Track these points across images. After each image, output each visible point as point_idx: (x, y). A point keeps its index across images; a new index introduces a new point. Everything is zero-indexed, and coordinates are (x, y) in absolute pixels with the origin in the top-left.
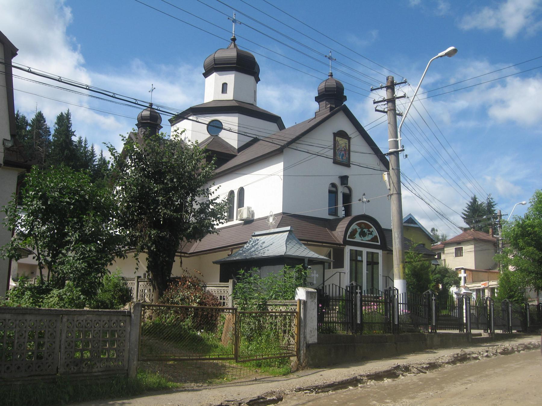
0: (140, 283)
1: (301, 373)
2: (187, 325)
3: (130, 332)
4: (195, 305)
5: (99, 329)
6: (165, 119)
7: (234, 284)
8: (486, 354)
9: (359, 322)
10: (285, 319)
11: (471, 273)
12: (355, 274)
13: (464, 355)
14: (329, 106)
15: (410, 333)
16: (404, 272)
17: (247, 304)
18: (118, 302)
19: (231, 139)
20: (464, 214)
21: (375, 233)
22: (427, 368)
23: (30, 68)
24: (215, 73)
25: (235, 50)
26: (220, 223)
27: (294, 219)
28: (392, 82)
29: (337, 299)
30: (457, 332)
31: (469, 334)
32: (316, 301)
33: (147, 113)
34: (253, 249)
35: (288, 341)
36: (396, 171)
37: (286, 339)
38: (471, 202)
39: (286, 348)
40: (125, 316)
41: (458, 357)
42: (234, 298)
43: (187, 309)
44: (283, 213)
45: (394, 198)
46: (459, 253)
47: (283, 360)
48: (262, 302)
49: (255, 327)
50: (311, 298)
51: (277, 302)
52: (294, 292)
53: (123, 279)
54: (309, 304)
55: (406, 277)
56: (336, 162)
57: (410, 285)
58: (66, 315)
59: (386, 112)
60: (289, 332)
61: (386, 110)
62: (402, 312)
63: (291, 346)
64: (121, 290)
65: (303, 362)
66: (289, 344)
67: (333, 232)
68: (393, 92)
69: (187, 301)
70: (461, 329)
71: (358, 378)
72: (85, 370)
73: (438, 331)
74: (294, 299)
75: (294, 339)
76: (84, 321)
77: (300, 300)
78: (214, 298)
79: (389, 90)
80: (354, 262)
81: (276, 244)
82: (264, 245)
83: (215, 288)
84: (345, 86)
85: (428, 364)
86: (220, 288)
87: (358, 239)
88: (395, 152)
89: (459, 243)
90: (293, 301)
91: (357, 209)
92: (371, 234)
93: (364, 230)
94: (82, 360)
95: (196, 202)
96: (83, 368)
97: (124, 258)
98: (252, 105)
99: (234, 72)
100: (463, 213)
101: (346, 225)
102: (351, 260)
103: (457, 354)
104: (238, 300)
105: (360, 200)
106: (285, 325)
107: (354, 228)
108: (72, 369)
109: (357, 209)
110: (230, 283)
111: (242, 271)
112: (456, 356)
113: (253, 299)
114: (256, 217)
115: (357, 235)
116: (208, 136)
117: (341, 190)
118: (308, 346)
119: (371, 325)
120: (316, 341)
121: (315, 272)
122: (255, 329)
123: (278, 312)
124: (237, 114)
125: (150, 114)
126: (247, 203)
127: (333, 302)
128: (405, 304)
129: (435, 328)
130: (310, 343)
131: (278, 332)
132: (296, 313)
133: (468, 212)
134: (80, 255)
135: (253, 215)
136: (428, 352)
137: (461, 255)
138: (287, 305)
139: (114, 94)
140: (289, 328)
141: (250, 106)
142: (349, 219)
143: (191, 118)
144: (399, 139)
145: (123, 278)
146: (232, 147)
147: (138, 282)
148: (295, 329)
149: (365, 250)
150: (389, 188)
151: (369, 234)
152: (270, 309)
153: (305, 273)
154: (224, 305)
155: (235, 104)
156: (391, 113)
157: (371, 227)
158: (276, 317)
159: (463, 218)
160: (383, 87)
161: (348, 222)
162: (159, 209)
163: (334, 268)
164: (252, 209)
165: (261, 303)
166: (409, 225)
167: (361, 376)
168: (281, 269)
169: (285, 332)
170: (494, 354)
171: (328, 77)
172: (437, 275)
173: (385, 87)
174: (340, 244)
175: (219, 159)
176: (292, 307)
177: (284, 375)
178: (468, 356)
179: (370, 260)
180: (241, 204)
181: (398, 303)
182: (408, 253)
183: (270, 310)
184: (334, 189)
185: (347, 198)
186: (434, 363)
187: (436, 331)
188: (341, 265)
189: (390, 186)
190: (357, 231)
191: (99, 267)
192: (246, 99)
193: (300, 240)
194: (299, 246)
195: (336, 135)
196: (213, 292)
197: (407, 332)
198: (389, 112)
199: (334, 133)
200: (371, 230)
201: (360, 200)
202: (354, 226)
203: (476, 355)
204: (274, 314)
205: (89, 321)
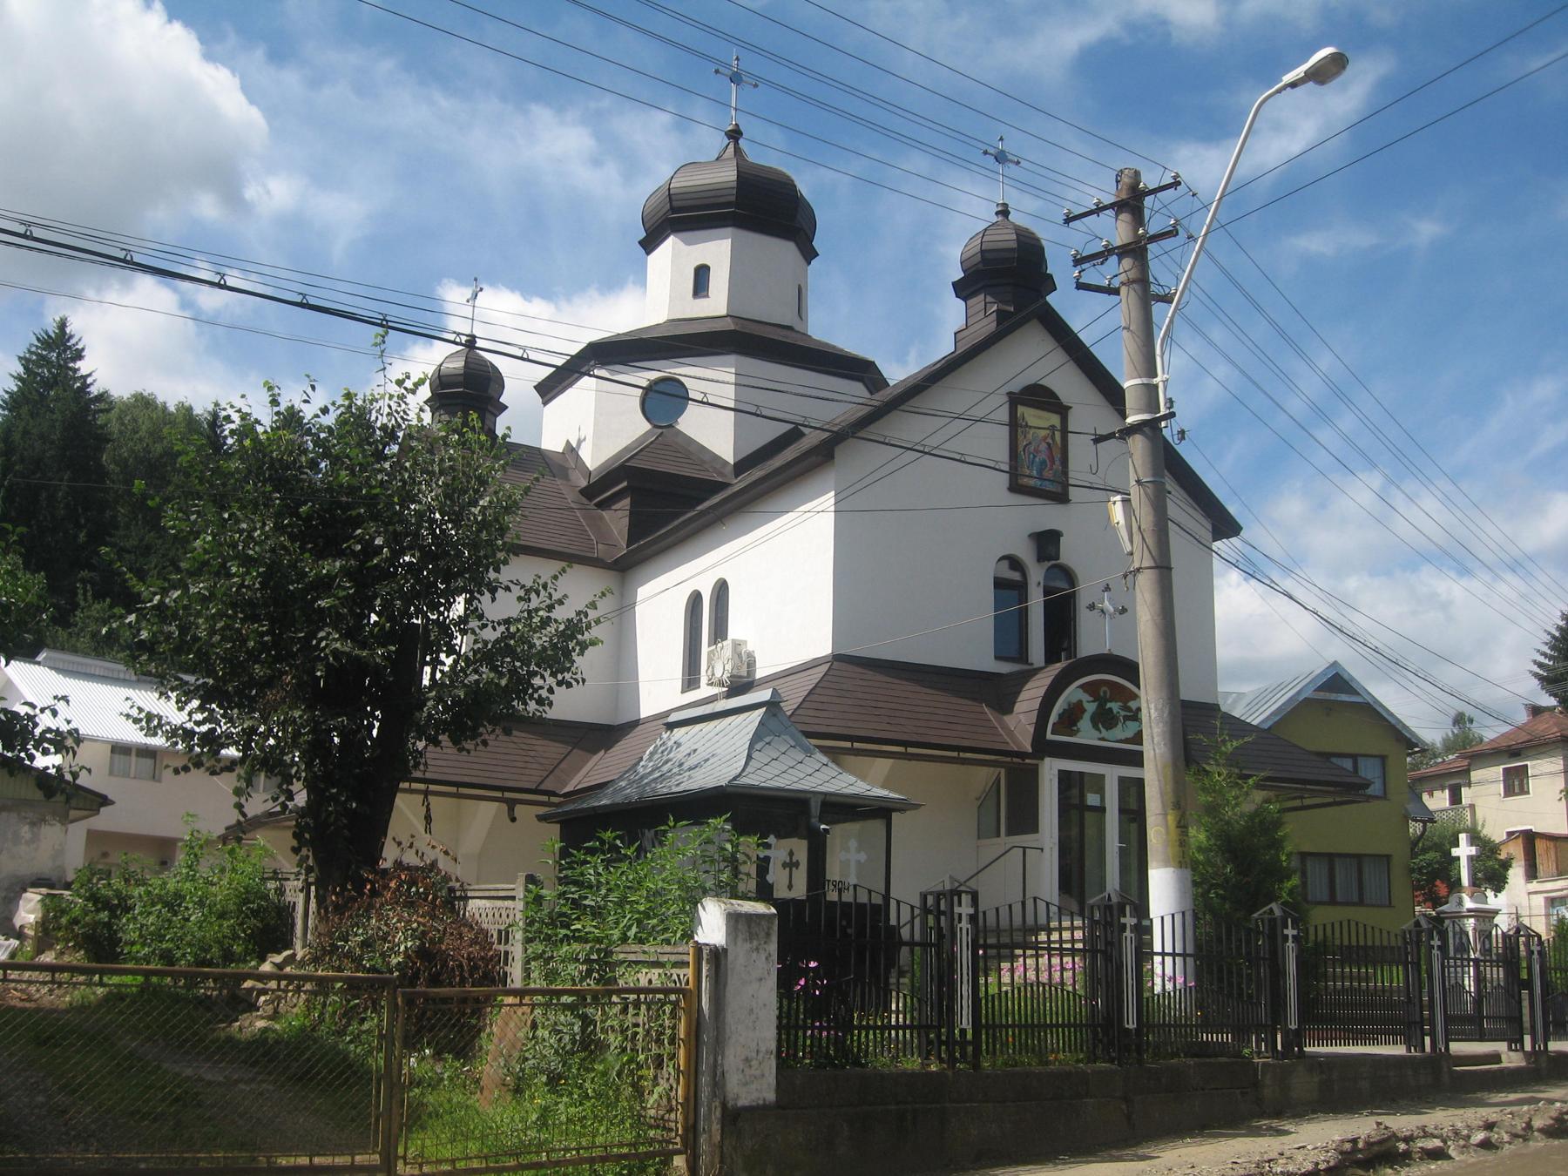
6: (518, 382)
8: (1479, 1136)
11: (1551, 844)
13: (1380, 1142)
15: (1191, 1061)
16: (1183, 843)
18: (246, 952)
19: (713, 431)
20: (1540, 665)
23: (304, 296)
26: (559, 684)
27: (869, 674)
30: (1399, 1050)
31: (1441, 1060)
32: (773, 947)
36: (1150, 489)
38: (1559, 628)
39: (660, 1123)
41: (1355, 1150)
44: (837, 658)
45: (1145, 585)
46: (1516, 783)
49: (573, 1042)
50: (752, 937)
54: (739, 959)
55: (1183, 859)
59: (1116, 292)
61: (1116, 283)
67: (1006, 718)
68: (1138, 218)
77: (699, 948)
79: (1125, 217)
81: (719, 755)
86: (499, 903)
87: (1086, 735)
88: (1144, 423)
89: (1514, 753)
93: (1109, 705)
98: (790, 328)
99: (729, 230)
100: (1535, 662)
101: (1042, 692)
103: (1354, 1141)
105: (1092, 607)
106: (659, 1042)
112: (1348, 1146)
115: (1085, 724)
116: (647, 426)
117: (1036, 574)
118: (733, 1117)
120: (771, 1096)
121: (853, 844)
124: (732, 358)
125: (466, 366)
126: (734, 631)
127: (1073, 941)
128: (1184, 955)
130: (743, 1102)
133: (1551, 658)
135: (751, 664)
136: (1256, 1132)
137: (1524, 791)
139: (29, 224)
141: (785, 332)
142: (1057, 668)
143: (596, 372)
146: (716, 458)
150: (1129, 548)
151: (1126, 718)
152: (626, 978)
155: (729, 325)
156: (1132, 293)
159: (1536, 675)
160: (1105, 208)
162: (322, 639)
163: (1010, 833)
164: (750, 648)
166: (1333, 696)
170: (1516, 1136)
171: (995, 219)
172: (1430, 855)
173: (1111, 206)
174: (1022, 755)
175: (664, 502)
178: (1402, 1146)
180: (720, 632)
184: (1016, 576)
187: (1301, 1049)
189: (1131, 541)
190: (1083, 711)
192: (771, 310)
193: (809, 735)
194: (800, 756)
195: (1015, 400)
198: (1124, 290)
202: (1072, 693)
203: (1437, 1143)
204: (632, 997)
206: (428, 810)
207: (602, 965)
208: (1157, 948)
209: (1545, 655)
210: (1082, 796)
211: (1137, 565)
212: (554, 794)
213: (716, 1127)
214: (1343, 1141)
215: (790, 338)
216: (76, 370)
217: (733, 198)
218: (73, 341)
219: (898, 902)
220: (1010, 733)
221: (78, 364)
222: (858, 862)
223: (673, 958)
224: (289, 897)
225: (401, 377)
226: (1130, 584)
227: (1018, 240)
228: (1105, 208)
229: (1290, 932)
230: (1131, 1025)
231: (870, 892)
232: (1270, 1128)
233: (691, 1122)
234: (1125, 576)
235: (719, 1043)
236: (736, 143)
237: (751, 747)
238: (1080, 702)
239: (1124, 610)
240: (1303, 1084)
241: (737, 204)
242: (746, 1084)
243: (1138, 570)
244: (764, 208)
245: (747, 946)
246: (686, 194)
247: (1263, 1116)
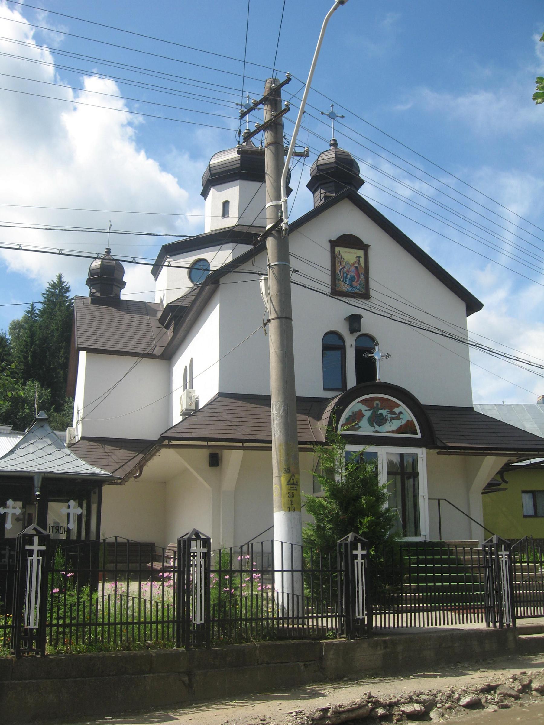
21: (408, 415)
24: (212, 189)
27: (239, 403)
87: (365, 429)
92: (398, 417)
107: (356, 409)
117: (350, 341)
128: (292, 571)
151: (392, 419)
157: (398, 406)
184: (335, 341)
190: (363, 416)
195: (334, 244)
199: (331, 241)
200: (397, 410)
216: (67, 297)
218: (65, 284)
221: (68, 294)
222: (14, 514)
227: (336, 157)
238: (360, 411)
239: (388, 356)
241: (241, 167)
246: (217, 166)
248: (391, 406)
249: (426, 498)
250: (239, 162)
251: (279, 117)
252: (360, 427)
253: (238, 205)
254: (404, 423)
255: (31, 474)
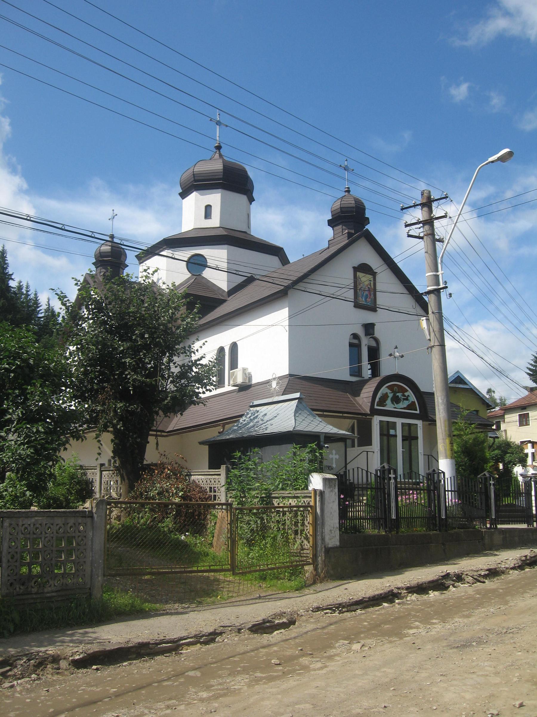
0: (104, 473)
1: (319, 586)
2: (167, 526)
3: (92, 539)
4: (177, 500)
5: (52, 535)
7: (228, 471)
9: (394, 517)
10: (296, 515)
12: (387, 453)
14: (347, 231)
15: (462, 530)
16: (452, 450)
17: (245, 497)
18: (76, 499)
19: (220, 280)
20: (530, 369)
21: (413, 398)
22: (485, 576)
25: (221, 161)
26: (207, 390)
27: (304, 382)
28: (429, 197)
29: (364, 488)
30: (524, 526)
33: (106, 248)
34: (252, 424)
35: (301, 545)
36: (437, 315)
37: (299, 541)
39: (299, 554)
40: (85, 517)
41: (526, 560)
42: (228, 489)
43: (166, 505)
44: (290, 375)
45: (436, 351)
46: (524, 421)
47: (295, 570)
48: (265, 494)
49: (257, 527)
50: (330, 487)
51: (286, 493)
52: (307, 479)
53: (81, 467)
54: (327, 495)
55: (454, 456)
56: (357, 306)
57: (461, 466)
58: (8, 517)
59: (422, 238)
60: (301, 533)
61: (422, 235)
62: (450, 503)
63: (305, 551)
64: (79, 483)
65: (322, 572)
66: (303, 549)
67: (356, 398)
68: (431, 211)
69: (167, 494)
70: (529, 523)
71: (395, 591)
72: (34, 590)
73: (499, 526)
74: (307, 489)
75: (309, 542)
76: (32, 526)
77: (315, 491)
78: (202, 491)
79: (425, 209)
80: (385, 438)
81: (281, 416)
82: (266, 418)
83: (203, 477)
84: (367, 205)
85: (487, 570)
87: (389, 406)
89: (524, 408)
90: (306, 491)
91: (388, 367)
92: (407, 399)
93: (398, 394)
94: (30, 576)
95: (174, 363)
96: (32, 587)
97: (83, 440)
99: (220, 190)
100: (528, 368)
101: (373, 389)
102: (382, 435)
103: (526, 556)
104: (234, 493)
105: (391, 355)
106: (296, 524)
108: (18, 589)
109: (388, 367)
110: (222, 470)
111: (238, 454)
112: (524, 558)
113: (254, 490)
114: (254, 381)
115: (389, 402)
116: (188, 275)
117: (365, 342)
118: (328, 551)
119: (410, 520)
120: (338, 544)
121: (334, 452)
122: (257, 530)
123: (286, 507)
124: (226, 246)
129: (494, 522)
130: (330, 546)
131: (287, 533)
132: (311, 507)
134: (25, 439)
135: (250, 379)
137: (527, 424)
138: (297, 497)
140: (302, 528)
142: (377, 380)
144: (440, 273)
145: (81, 466)
146: (220, 289)
147: (101, 471)
148: (309, 529)
149: (399, 421)
150: (429, 338)
151: (404, 399)
152: (275, 502)
153: (321, 454)
154: (215, 499)
156: (429, 239)
157: (407, 391)
158: (284, 513)
159: (528, 374)
160: (417, 205)
161: (375, 385)
162: (127, 375)
163: (359, 446)
164: (249, 371)
165: (263, 495)
167: (398, 588)
168: (289, 449)
169: (296, 533)
171: (344, 194)
172: (496, 452)
173: (420, 204)
174: (366, 415)
175: (203, 306)
176: (305, 500)
177: (297, 590)
179: (406, 434)
180: (234, 365)
181: (445, 491)
182: (457, 423)
183: (276, 505)
184: (356, 341)
185: (374, 353)
186: (495, 569)
187: (496, 526)
188: (369, 442)
191: (49, 453)
194: (312, 419)
196: (201, 482)
197: (458, 528)
198: (425, 238)
199: (354, 268)
200: (406, 394)
201: (391, 355)
202: (384, 390)
204: (281, 509)
205: (38, 526)
206: (157, 441)
207: (267, 500)
208: (447, 489)
209: (531, 365)
210: (388, 432)
211: (432, 345)
212: (164, 432)
213: (323, 554)
214: (521, 557)
215: (242, 236)
217: (221, 176)
219: (371, 473)
220: (360, 406)
222: (336, 458)
223: (303, 495)
224: (90, 476)
225: (146, 268)
226: (430, 352)
228: (417, 205)
229: (492, 482)
230: (444, 517)
231: (362, 469)
232: (491, 554)
233: (315, 553)
234: (428, 349)
235: (323, 524)
236: (220, 152)
237: (295, 415)
238: (387, 393)
240: (498, 539)
242: (331, 539)
243: (433, 346)
244: (235, 181)
245: (329, 490)
246: (200, 174)
247: (486, 550)
248: (404, 391)
249: (422, 454)
250: (222, 174)
251: (427, 220)
252: (386, 405)
253: (220, 210)
254: (410, 402)
255: (318, 434)
